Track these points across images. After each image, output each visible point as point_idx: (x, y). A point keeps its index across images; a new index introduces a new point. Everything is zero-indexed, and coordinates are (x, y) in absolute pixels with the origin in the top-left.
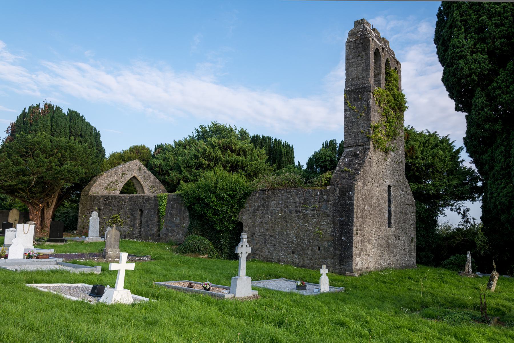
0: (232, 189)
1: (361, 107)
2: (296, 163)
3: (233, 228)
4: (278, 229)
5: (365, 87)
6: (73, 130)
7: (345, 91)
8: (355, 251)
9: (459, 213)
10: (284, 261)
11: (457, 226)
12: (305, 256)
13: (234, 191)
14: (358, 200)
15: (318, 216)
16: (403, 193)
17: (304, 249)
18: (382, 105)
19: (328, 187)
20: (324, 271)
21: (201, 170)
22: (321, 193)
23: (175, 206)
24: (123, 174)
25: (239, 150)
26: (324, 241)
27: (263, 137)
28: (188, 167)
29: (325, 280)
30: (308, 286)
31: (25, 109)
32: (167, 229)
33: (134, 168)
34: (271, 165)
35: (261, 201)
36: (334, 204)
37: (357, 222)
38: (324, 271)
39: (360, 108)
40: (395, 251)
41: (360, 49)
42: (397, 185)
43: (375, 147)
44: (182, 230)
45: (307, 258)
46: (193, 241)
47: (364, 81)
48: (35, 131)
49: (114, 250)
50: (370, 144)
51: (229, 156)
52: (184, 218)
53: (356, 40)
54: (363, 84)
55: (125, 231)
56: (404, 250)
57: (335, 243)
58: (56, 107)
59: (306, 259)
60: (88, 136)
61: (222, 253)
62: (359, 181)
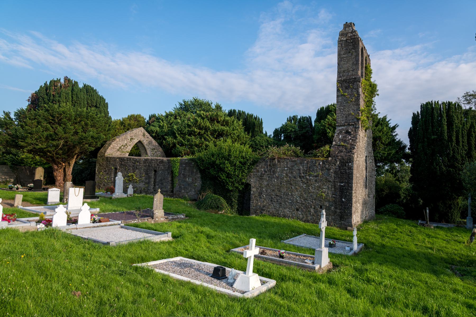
0: (243, 157)
1: (352, 95)
2: (264, 133)
4: (284, 190)
5: (355, 78)
17: (307, 207)
19: (330, 159)
21: (193, 137)
23: (188, 168)
24: (131, 139)
25: (223, 121)
26: (326, 201)
28: (182, 134)
31: (46, 82)
32: (180, 187)
33: (139, 134)
34: (248, 133)
35: (267, 167)
36: (335, 172)
44: (195, 188)
45: (310, 214)
46: (212, 200)
47: (354, 73)
48: (59, 102)
52: (196, 179)
54: (353, 75)
55: (140, 187)
57: (336, 203)
58: (74, 81)
59: (309, 215)
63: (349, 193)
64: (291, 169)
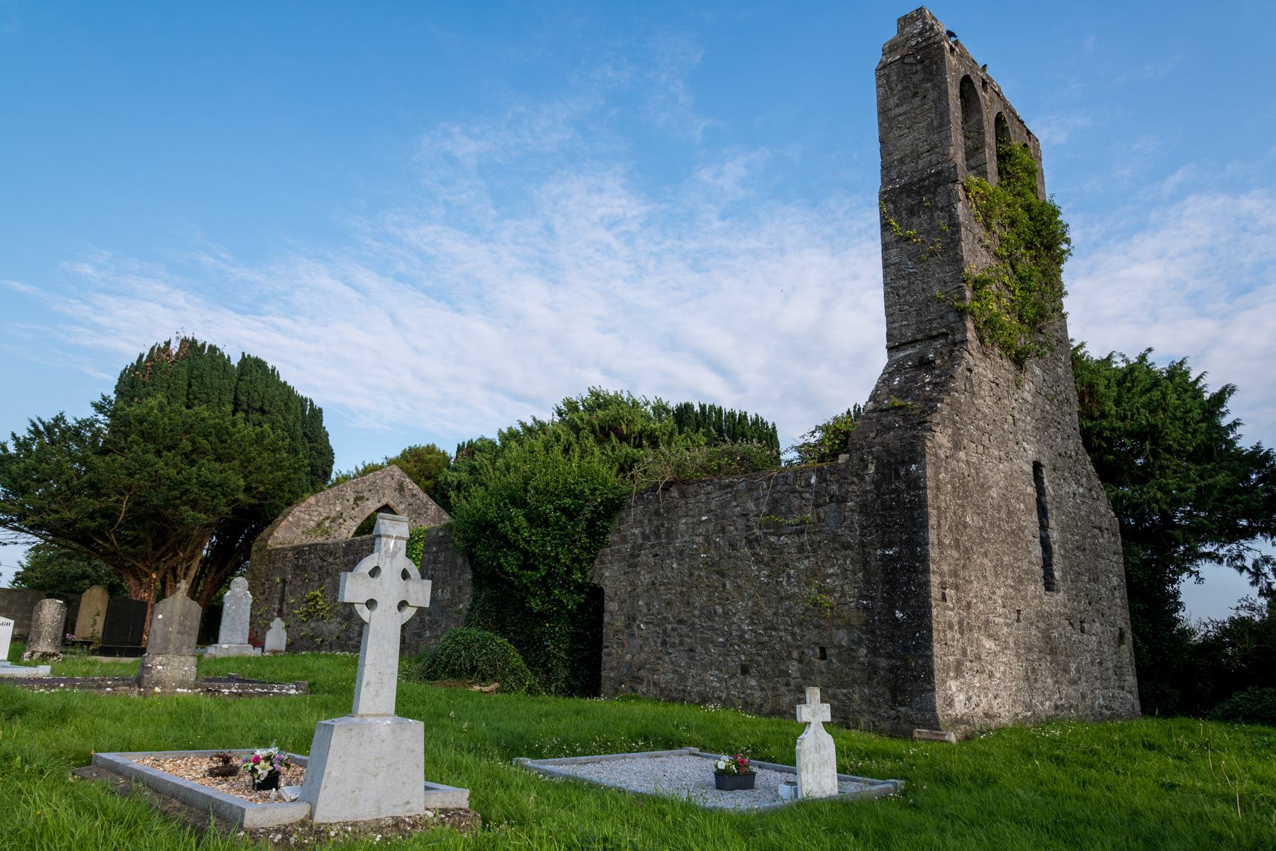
0: (570, 493)
1: (932, 230)
3: (580, 605)
4: (699, 600)
5: (939, 173)
6: (243, 398)
7: (882, 194)
8: (942, 655)
9: (1242, 569)
10: (719, 698)
11: (1233, 614)
12: (782, 680)
13: (576, 497)
14: (938, 488)
15: (814, 551)
16: (1081, 490)
18: (995, 228)
19: (842, 458)
20: (814, 711)
22: (822, 479)
24: (356, 499)
27: (703, 408)
29: (818, 748)
30: (764, 775)
35: (650, 520)
36: (863, 509)
37: (941, 562)
38: (814, 711)
39: (928, 232)
40: (1073, 666)
41: (917, 78)
42: (1059, 463)
43: (981, 340)
45: (787, 684)
46: (458, 643)
47: (934, 157)
49: (176, 661)
50: (965, 329)
51: (613, 449)
52: (460, 588)
53: (902, 58)
54: (931, 166)
56: (1101, 663)
57: (872, 632)
59: (783, 689)
60: (279, 411)
61: (548, 679)
62: (938, 430)
63: (919, 585)
64: (720, 517)
